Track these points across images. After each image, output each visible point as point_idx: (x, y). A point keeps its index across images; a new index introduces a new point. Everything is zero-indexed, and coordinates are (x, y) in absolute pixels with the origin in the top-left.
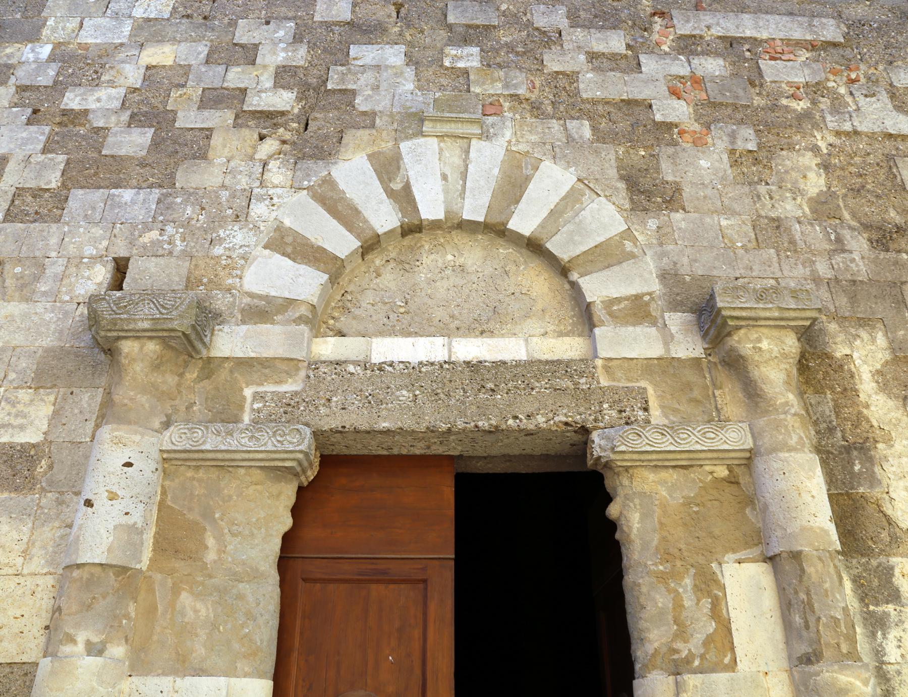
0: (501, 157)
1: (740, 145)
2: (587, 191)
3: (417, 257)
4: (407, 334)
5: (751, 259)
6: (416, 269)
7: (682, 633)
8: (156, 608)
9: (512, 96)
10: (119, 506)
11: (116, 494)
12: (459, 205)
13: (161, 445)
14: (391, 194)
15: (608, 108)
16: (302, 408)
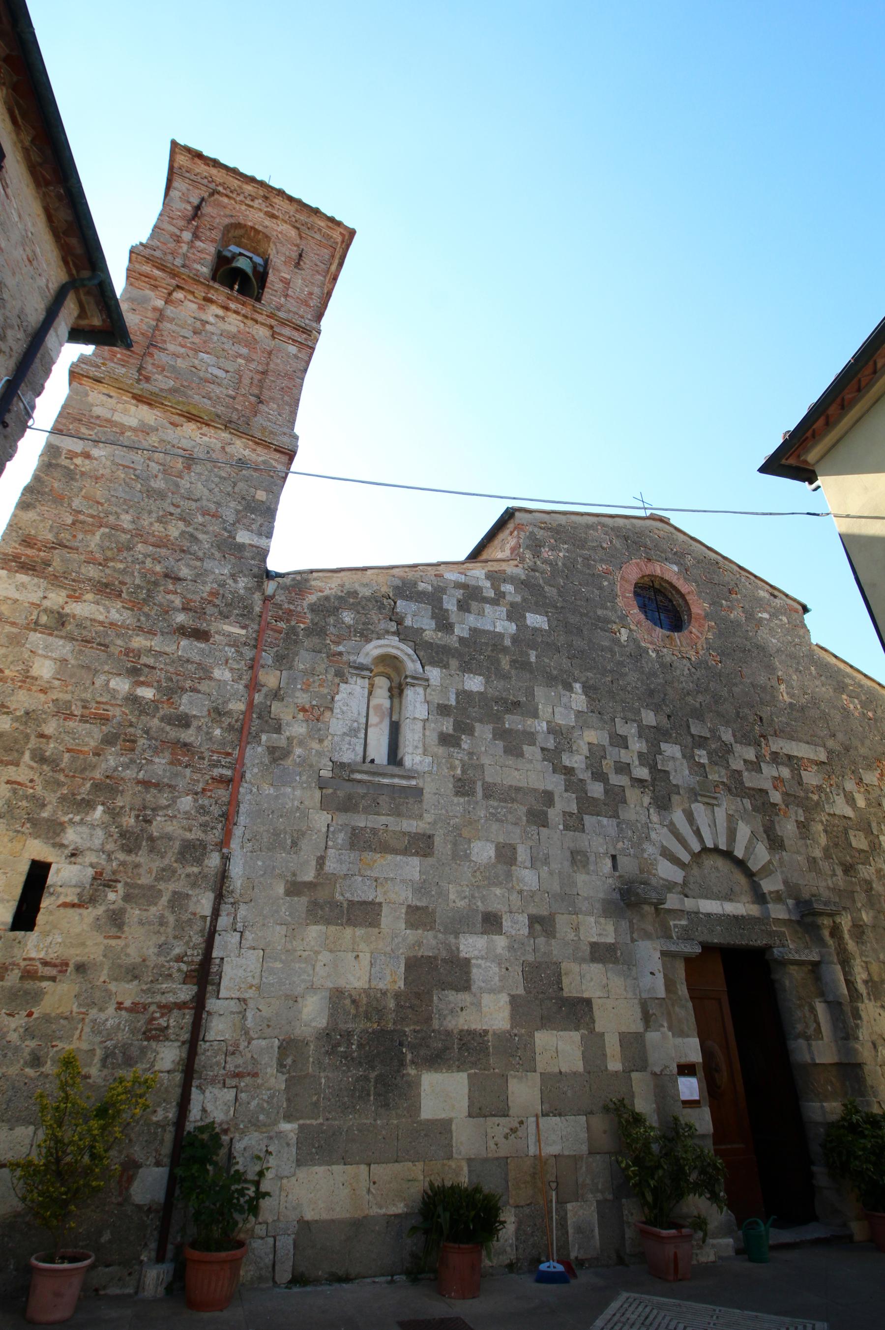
7: (807, 1026)
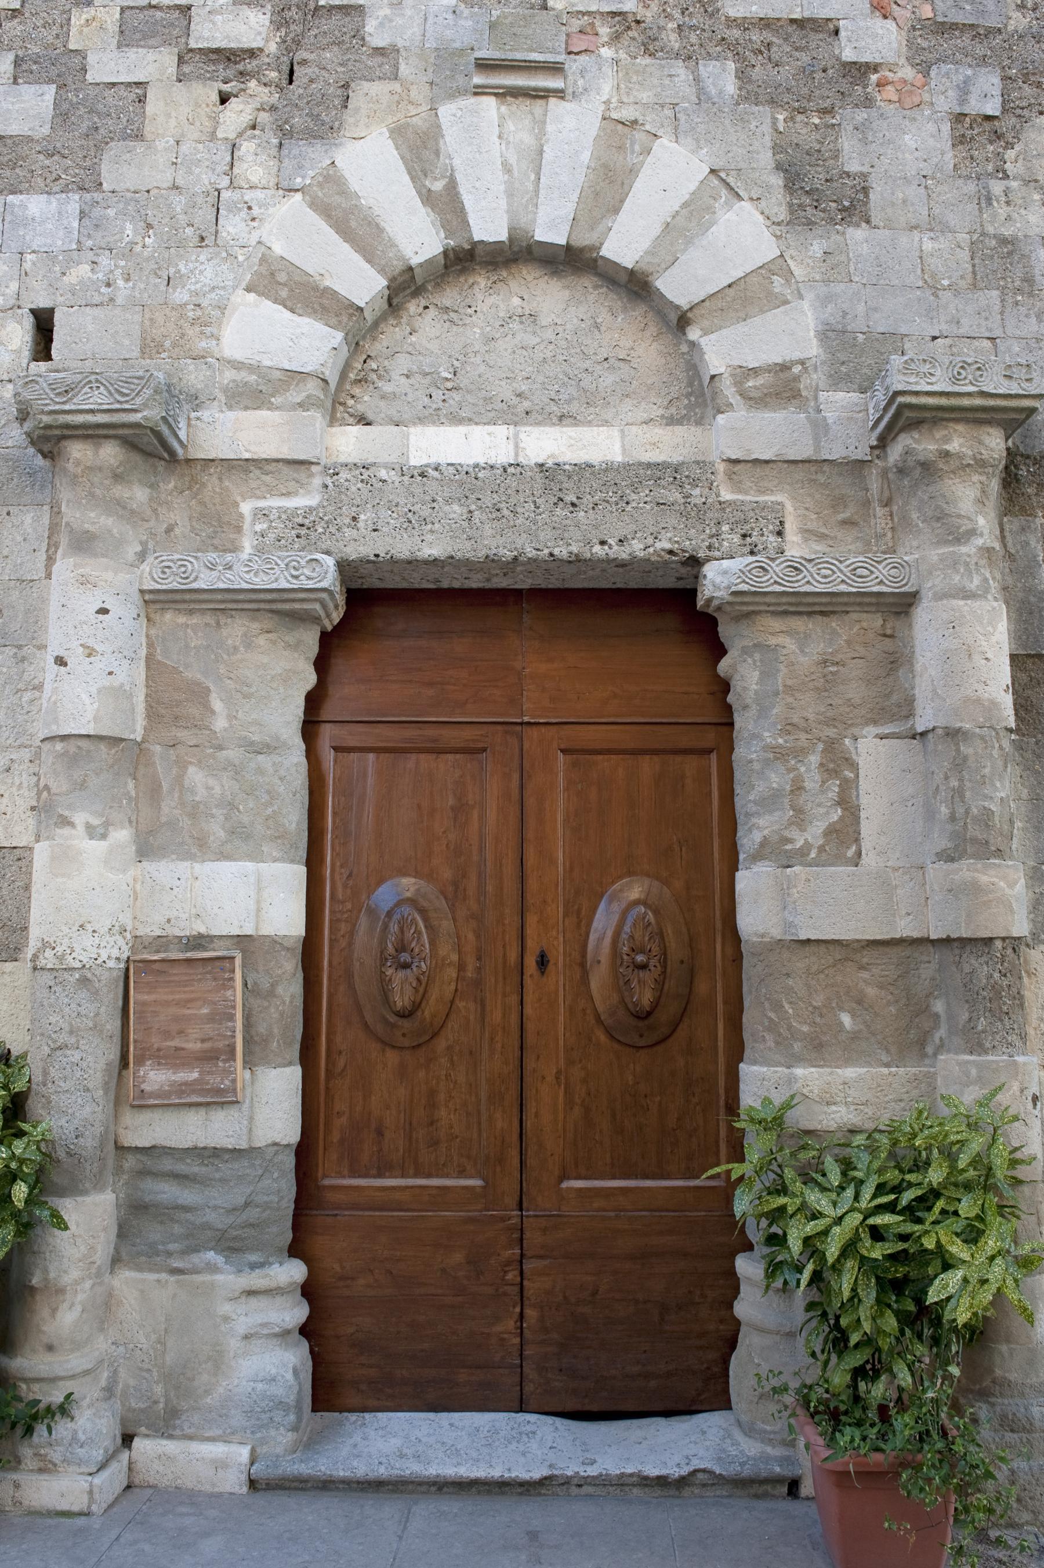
0: (594, 132)
1: (976, 106)
2: (724, 192)
3: (468, 301)
4: (456, 420)
5: (960, 306)
6: (468, 320)
7: (800, 818)
8: (160, 786)
9: (614, 14)
10: (100, 664)
11: (93, 649)
12: (530, 216)
13: (141, 584)
14: (428, 198)
15: (768, 36)
16: (320, 530)
